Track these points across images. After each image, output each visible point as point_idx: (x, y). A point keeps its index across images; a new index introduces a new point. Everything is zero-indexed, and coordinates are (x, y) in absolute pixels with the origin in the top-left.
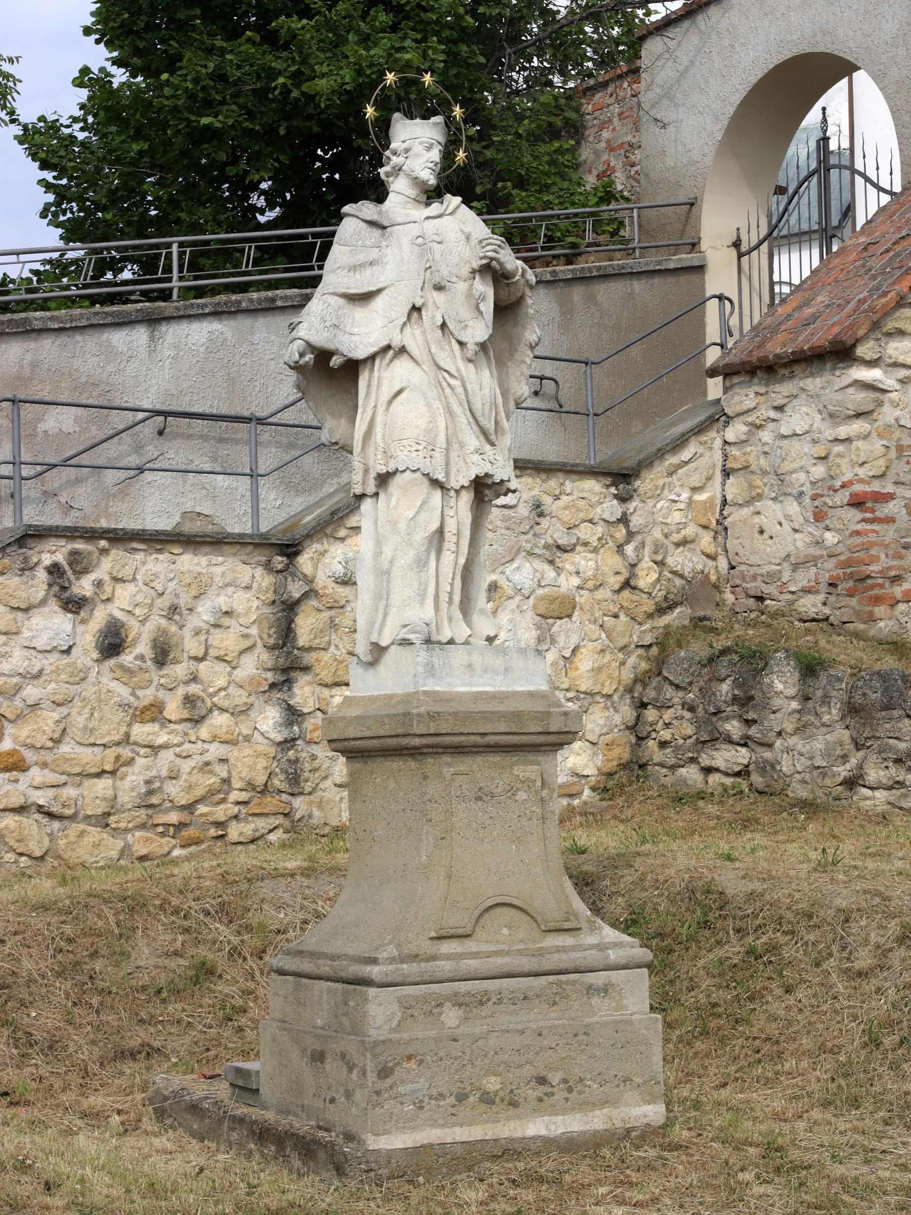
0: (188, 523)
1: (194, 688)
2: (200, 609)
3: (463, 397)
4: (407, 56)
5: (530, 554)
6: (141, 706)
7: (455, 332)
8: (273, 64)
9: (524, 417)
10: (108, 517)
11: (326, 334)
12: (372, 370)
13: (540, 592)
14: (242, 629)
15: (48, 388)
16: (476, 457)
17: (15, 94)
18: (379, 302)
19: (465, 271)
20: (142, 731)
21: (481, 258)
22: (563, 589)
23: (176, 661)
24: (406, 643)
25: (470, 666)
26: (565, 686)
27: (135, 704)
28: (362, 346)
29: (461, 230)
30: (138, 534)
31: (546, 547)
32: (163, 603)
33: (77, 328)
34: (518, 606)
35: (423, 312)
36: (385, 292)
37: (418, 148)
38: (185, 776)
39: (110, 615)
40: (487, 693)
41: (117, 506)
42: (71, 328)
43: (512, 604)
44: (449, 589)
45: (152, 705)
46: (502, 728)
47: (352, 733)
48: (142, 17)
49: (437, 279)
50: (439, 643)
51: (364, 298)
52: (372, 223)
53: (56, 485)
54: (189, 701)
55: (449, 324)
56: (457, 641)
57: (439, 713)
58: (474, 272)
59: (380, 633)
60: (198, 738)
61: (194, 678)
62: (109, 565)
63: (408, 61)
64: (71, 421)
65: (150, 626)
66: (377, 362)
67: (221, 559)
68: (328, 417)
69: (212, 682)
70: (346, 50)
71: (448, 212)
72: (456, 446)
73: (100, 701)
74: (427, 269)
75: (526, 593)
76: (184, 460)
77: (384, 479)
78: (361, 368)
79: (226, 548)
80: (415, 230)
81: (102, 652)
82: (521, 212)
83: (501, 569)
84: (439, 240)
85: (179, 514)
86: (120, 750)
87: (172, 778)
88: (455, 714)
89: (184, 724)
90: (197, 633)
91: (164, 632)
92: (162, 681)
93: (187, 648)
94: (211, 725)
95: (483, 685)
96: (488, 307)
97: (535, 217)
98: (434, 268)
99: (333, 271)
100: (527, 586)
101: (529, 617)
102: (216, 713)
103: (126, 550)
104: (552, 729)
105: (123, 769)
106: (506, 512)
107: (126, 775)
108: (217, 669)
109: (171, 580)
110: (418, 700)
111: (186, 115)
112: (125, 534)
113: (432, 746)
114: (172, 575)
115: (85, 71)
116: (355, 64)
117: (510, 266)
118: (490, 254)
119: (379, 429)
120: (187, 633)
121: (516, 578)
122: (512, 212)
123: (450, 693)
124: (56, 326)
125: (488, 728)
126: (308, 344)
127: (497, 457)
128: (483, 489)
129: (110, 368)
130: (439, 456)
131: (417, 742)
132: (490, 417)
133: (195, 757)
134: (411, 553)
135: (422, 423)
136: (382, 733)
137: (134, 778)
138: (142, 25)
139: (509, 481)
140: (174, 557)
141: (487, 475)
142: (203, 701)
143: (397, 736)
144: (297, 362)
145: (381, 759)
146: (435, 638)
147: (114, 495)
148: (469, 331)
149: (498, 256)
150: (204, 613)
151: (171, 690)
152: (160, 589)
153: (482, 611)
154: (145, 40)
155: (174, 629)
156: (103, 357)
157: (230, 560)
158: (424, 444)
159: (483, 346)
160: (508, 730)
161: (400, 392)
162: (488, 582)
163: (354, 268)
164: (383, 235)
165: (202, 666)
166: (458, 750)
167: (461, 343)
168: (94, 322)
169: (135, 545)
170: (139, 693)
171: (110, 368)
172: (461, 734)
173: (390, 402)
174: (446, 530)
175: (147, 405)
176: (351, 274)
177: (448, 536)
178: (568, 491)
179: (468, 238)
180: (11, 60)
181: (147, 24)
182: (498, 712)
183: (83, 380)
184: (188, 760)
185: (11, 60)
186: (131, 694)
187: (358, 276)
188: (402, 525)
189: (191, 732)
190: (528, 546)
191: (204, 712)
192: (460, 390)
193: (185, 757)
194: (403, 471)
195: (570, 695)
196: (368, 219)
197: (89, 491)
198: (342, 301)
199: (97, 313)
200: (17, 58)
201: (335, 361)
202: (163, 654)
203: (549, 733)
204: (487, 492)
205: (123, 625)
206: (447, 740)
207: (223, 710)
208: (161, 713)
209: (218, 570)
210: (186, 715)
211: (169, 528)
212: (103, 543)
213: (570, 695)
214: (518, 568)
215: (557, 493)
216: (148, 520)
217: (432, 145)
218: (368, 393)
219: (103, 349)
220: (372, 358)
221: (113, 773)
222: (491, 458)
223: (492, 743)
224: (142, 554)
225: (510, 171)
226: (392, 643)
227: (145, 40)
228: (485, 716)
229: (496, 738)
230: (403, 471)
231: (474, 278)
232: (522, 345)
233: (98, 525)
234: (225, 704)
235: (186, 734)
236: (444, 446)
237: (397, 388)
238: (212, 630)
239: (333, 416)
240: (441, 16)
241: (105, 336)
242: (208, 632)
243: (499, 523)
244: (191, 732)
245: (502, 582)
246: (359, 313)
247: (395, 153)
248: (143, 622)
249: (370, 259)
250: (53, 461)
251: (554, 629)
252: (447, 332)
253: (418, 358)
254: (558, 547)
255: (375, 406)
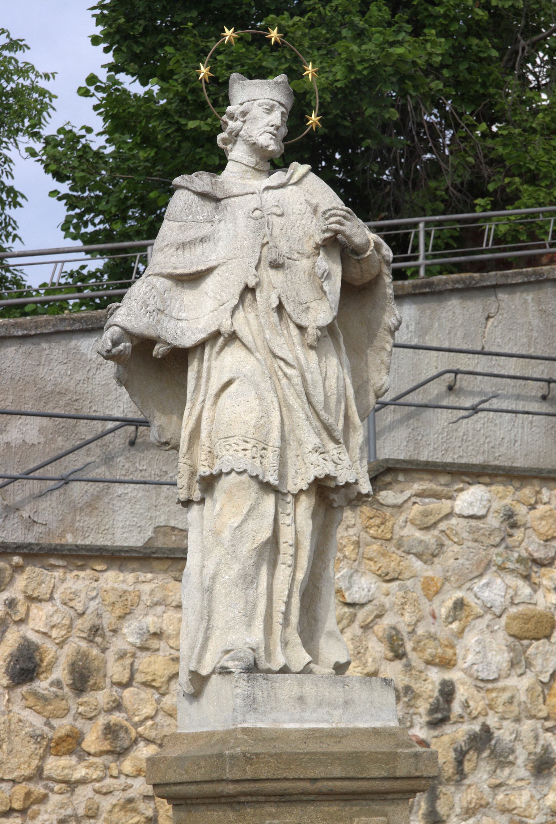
0: (161, 537)
1: (117, 717)
2: (125, 630)
3: (300, 388)
4: (400, 50)
5: (501, 568)
6: (55, 737)
7: (294, 317)
8: (264, 64)
9: (531, 422)
10: (74, 532)
11: (145, 320)
12: (201, 360)
13: (513, 610)
14: (172, 651)
15: (11, 398)
16: (315, 457)
17: (50, 110)
18: (210, 283)
19: (309, 247)
20: (55, 765)
21: (324, 232)
22: (540, 607)
23: (97, 688)
24: (225, 671)
25: (301, 699)
26: (543, 714)
27: (50, 735)
28: (189, 333)
29: (307, 200)
30: (55, 549)
31: (520, 560)
32: (83, 624)
33: (42, 335)
34: (488, 626)
35: (258, 293)
36: (216, 272)
37: (256, 111)
38: (104, 815)
39: (24, 638)
40: (321, 730)
41: (84, 521)
42: (35, 335)
43: (482, 624)
44: (283, 608)
45: (68, 736)
46: (337, 772)
47: (172, 777)
48: (141, 22)
49: (274, 256)
50: (269, 671)
51: (192, 279)
52: (204, 196)
53: (18, 499)
54: (111, 731)
55: (286, 306)
56: (293, 669)
57: (257, 755)
58: (318, 247)
59: (200, 659)
60: (120, 772)
61: (118, 706)
62: (24, 583)
63: (400, 55)
64: (35, 432)
65: (68, 649)
66: (207, 350)
67: (149, 576)
68: (157, 414)
69: (138, 710)
70: (339, 46)
71: (293, 181)
72: (293, 444)
73: (9, 732)
74: (263, 245)
75: (497, 611)
76: (157, 471)
77: (209, 483)
78: (190, 358)
79: (155, 564)
80: (252, 202)
81: (12, 678)
82: (527, 207)
83: (468, 585)
84: (279, 212)
85: (151, 529)
86: (31, 786)
87: (90, 817)
88: (278, 755)
89: (105, 757)
90: (122, 656)
91: (85, 656)
92: (81, 709)
93: (109, 674)
94: (136, 758)
95: (318, 721)
96: (334, 286)
97: (543, 212)
98: (271, 244)
99: (161, 250)
100: (498, 603)
101: (501, 638)
102: (142, 744)
103: (43, 567)
104: (398, 774)
105: (35, 807)
106: (474, 523)
107: (37, 813)
108: (143, 695)
109: (93, 599)
110: (236, 738)
111: (176, 118)
112: (41, 549)
113: (250, 794)
114: (94, 594)
115: (92, 79)
116: (347, 60)
117: (358, 240)
118: (333, 226)
119: (204, 425)
120: (111, 656)
121: (486, 594)
122: (519, 208)
123: (276, 731)
124: (20, 333)
125: (319, 772)
126: (125, 331)
127: (342, 456)
128: (327, 495)
129: (78, 377)
130: (272, 457)
131: (231, 789)
132: (338, 412)
133: (116, 793)
134: (237, 567)
135: (252, 418)
136: (199, 778)
137: (46, 817)
138: (141, 29)
139: (356, 483)
140: (97, 574)
141: (328, 477)
142: (127, 731)
143: (212, 781)
144: (109, 351)
145: (203, 808)
146: (263, 664)
147: (82, 509)
148: (312, 314)
149: (343, 228)
150: (130, 634)
151: (90, 719)
152: (80, 607)
153: (331, 634)
154: (143, 45)
155: (95, 651)
156: (71, 365)
157: (161, 576)
158: (253, 442)
159: (329, 330)
160: (344, 775)
161: (228, 384)
162: (454, 599)
163: (183, 246)
164: (217, 208)
165: (127, 693)
166: (284, 799)
167: (302, 329)
168: (61, 328)
169: (53, 561)
170: (55, 723)
171: (78, 377)
172: (286, 779)
173: (218, 395)
174: (282, 540)
175: (118, 414)
176: (180, 252)
177: (283, 547)
178: (545, 499)
179: (315, 210)
180: (47, 77)
181: (145, 29)
182: (332, 754)
183: (49, 389)
184: (109, 797)
185: (47, 77)
186: (45, 724)
187: (187, 254)
188: (226, 535)
189: (113, 765)
190: (499, 560)
191: (127, 743)
192: (297, 380)
193: (106, 794)
194: (228, 473)
195: (548, 724)
196: (200, 190)
197: (54, 505)
198: (168, 283)
199: (64, 320)
200: (53, 74)
201: (158, 350)
202: (82, 678)
203: (396, 778)
204: (334, 496)
205: (37, 648)
206: (269, 787)
207: (149, 741)
208: (79, 744)
209: (147, 588)
210: (107, 746)
211: (140, 544)
212: (16, 559)
213: (548, 724)
214: (487, 584)
215: (532, 501)
216: (118, 535)
217: (273, 107)
218: (197, 387)
219: (71, 357)
220: (201, 345)
221: (23, 811)
222: (335, 458)
223: (325, 790)
224: (61, 570)
225: (520, 167)
226: (213, 672)
227: (143, 45)
228: (315, 758)
229: (330, 784)
230: (228, 473)
231: (319, 254)
232: (381, 330)
233: (63, 542)
234: (152, 734)
235: (107, 768)
236: (278, 444)
237: (225, 379)
238: (139, 654)
239: (164, 413)
240: (449, 10)
241: (73, 343)
242: (134, 656)
243: (465, 535)
244: (113, 765)
245: (470, 599)
246: (188, 295)
247: (232, 117)
248: (61, 645)
249: (201, 235)
250: (15, 474)
251: (531, 651)
252: (285, 316)
253: (250, 344)
254: (535, 561)
255: (204, 401)
